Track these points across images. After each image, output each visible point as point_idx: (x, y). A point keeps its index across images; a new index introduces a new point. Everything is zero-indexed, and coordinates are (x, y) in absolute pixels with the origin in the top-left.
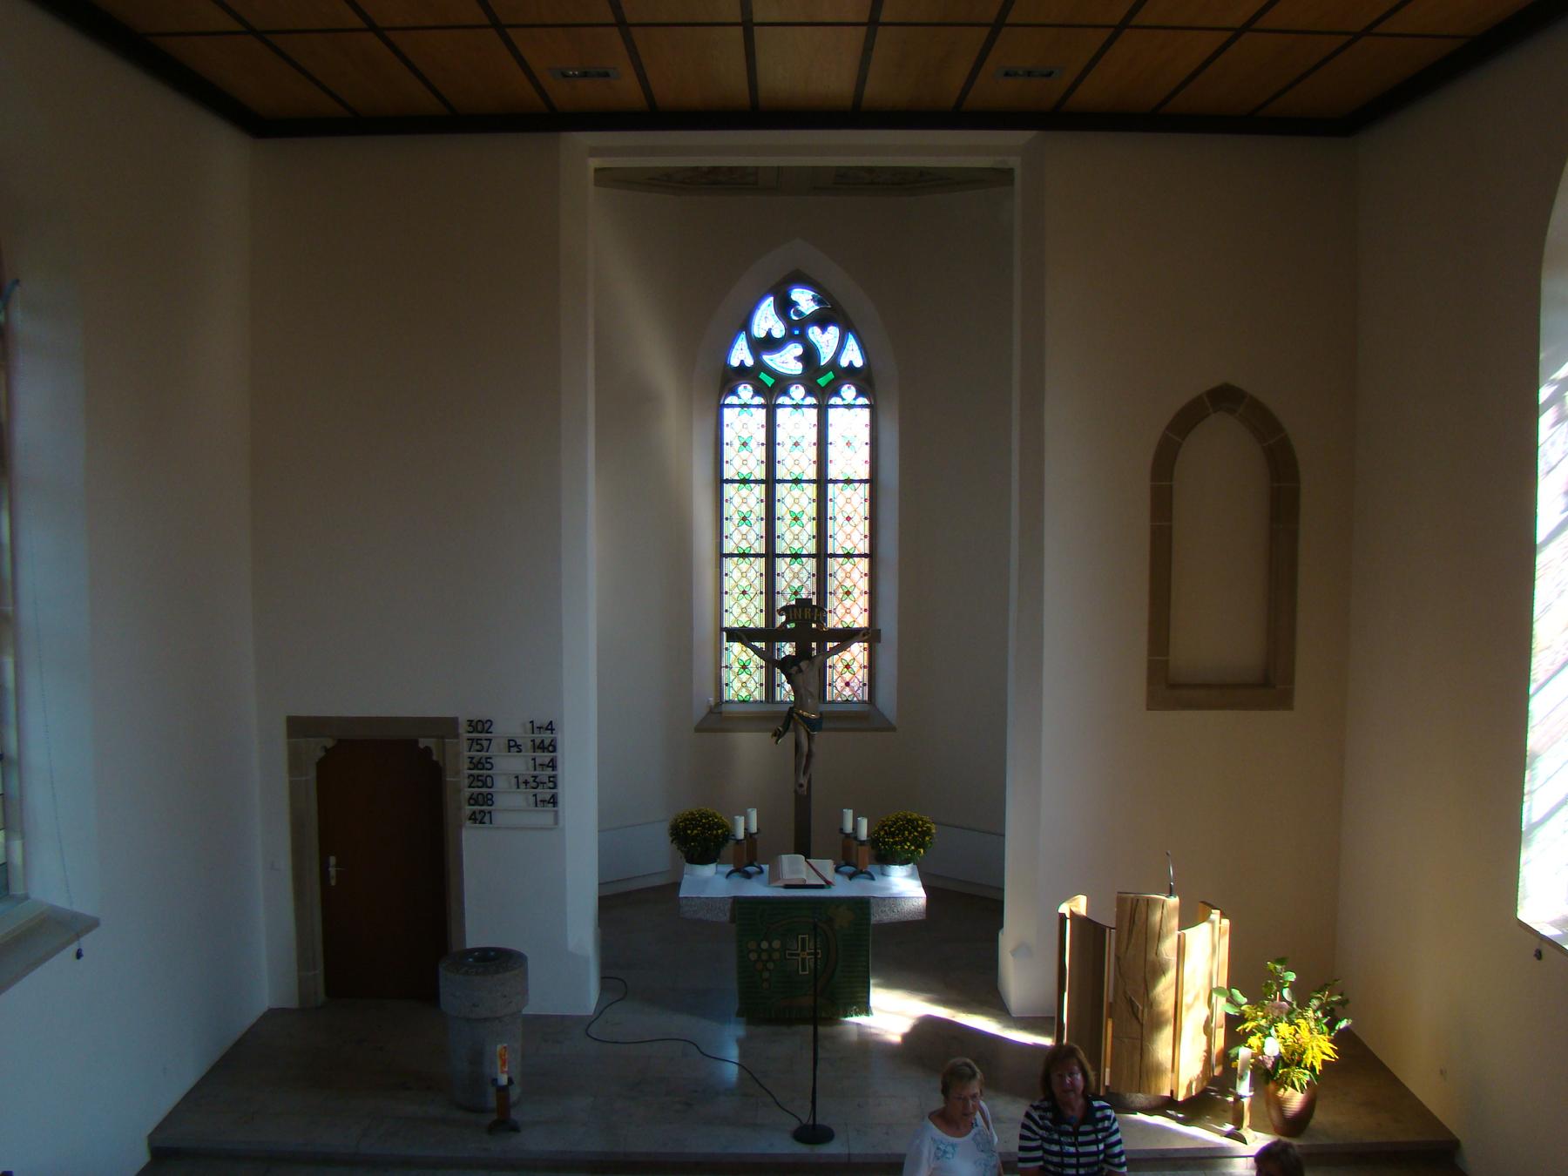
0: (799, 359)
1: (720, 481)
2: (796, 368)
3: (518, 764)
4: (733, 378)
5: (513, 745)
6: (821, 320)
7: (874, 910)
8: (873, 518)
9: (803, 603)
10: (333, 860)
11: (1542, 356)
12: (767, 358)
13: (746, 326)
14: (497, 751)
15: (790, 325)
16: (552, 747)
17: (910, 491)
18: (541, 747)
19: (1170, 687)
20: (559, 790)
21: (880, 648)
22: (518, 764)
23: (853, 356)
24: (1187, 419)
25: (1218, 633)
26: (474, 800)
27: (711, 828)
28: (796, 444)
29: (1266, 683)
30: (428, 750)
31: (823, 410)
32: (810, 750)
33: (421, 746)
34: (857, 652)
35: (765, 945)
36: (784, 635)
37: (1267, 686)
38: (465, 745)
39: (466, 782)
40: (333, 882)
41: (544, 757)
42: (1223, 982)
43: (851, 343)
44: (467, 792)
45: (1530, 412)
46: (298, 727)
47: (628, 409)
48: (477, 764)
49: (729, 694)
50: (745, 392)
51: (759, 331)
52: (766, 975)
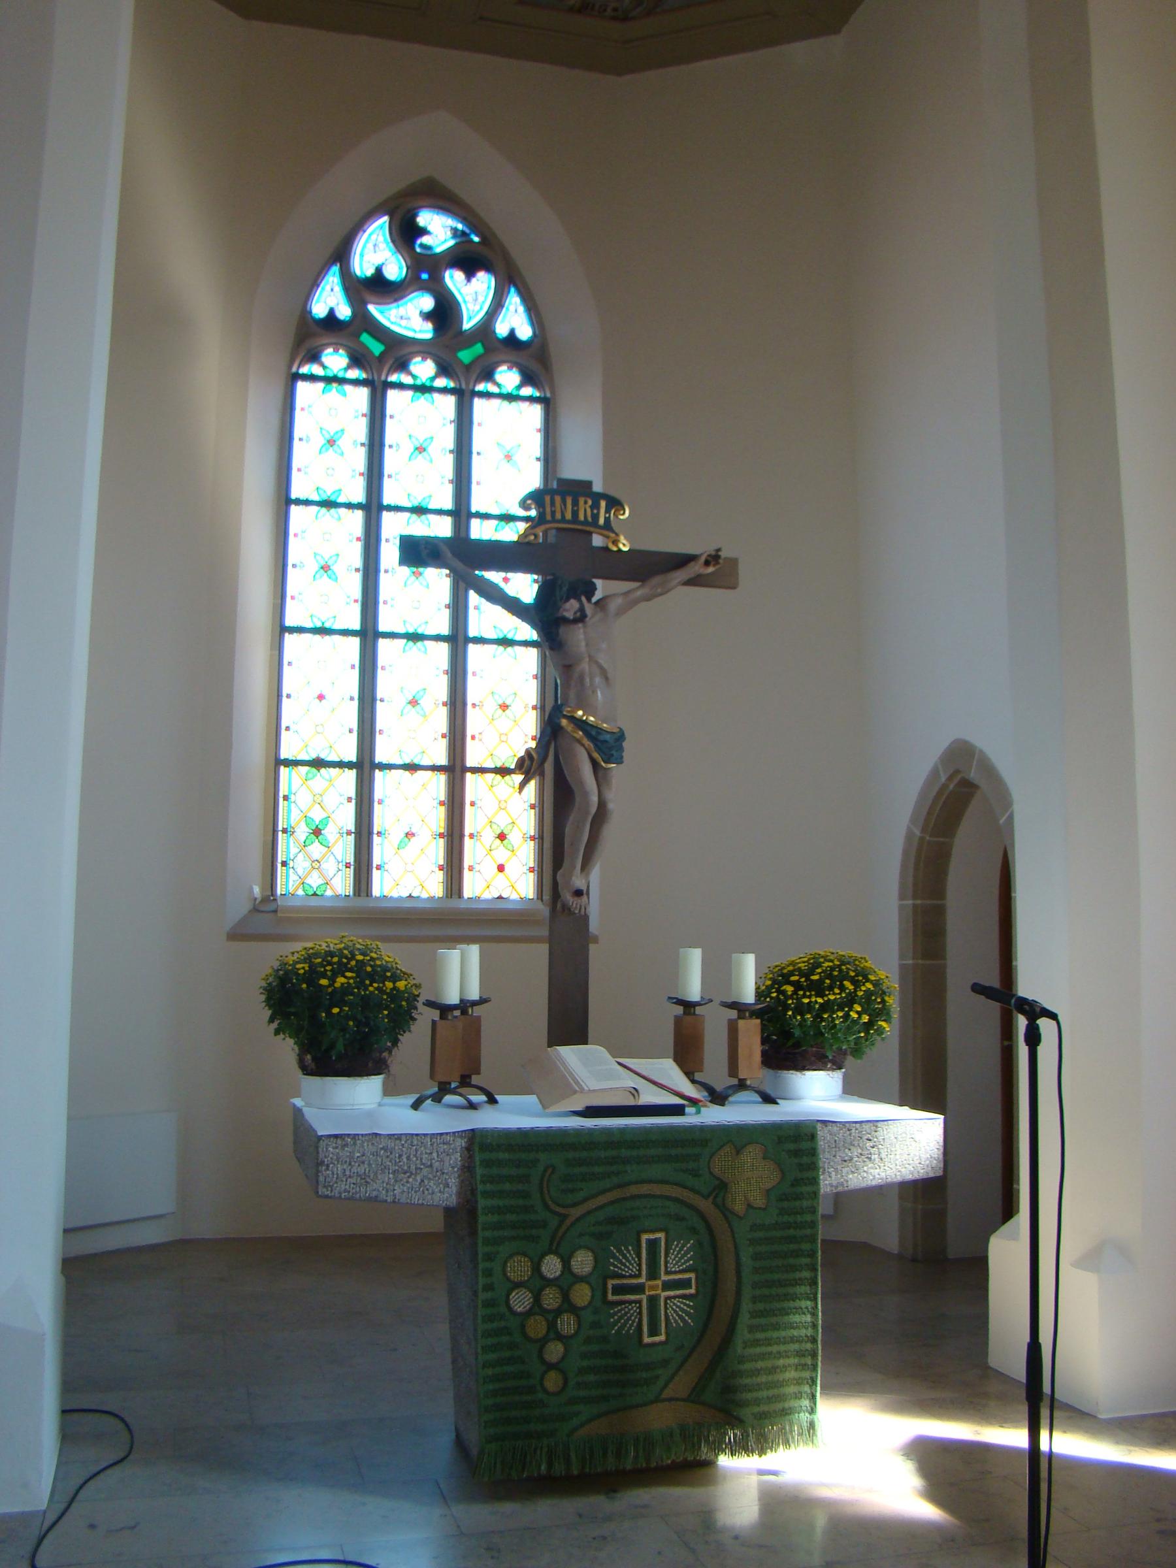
0: (428, 316)
1: (284, 501)
2: (425, 331)
4: (310, 336)
6: (468, 261)
13: (342, 255)
23: (515, 320)
32: (602, 805)
35: (552, 1266)
43: (514, 301)
49: (288, 883)
50: (335, 360)
52: (555, 1351)
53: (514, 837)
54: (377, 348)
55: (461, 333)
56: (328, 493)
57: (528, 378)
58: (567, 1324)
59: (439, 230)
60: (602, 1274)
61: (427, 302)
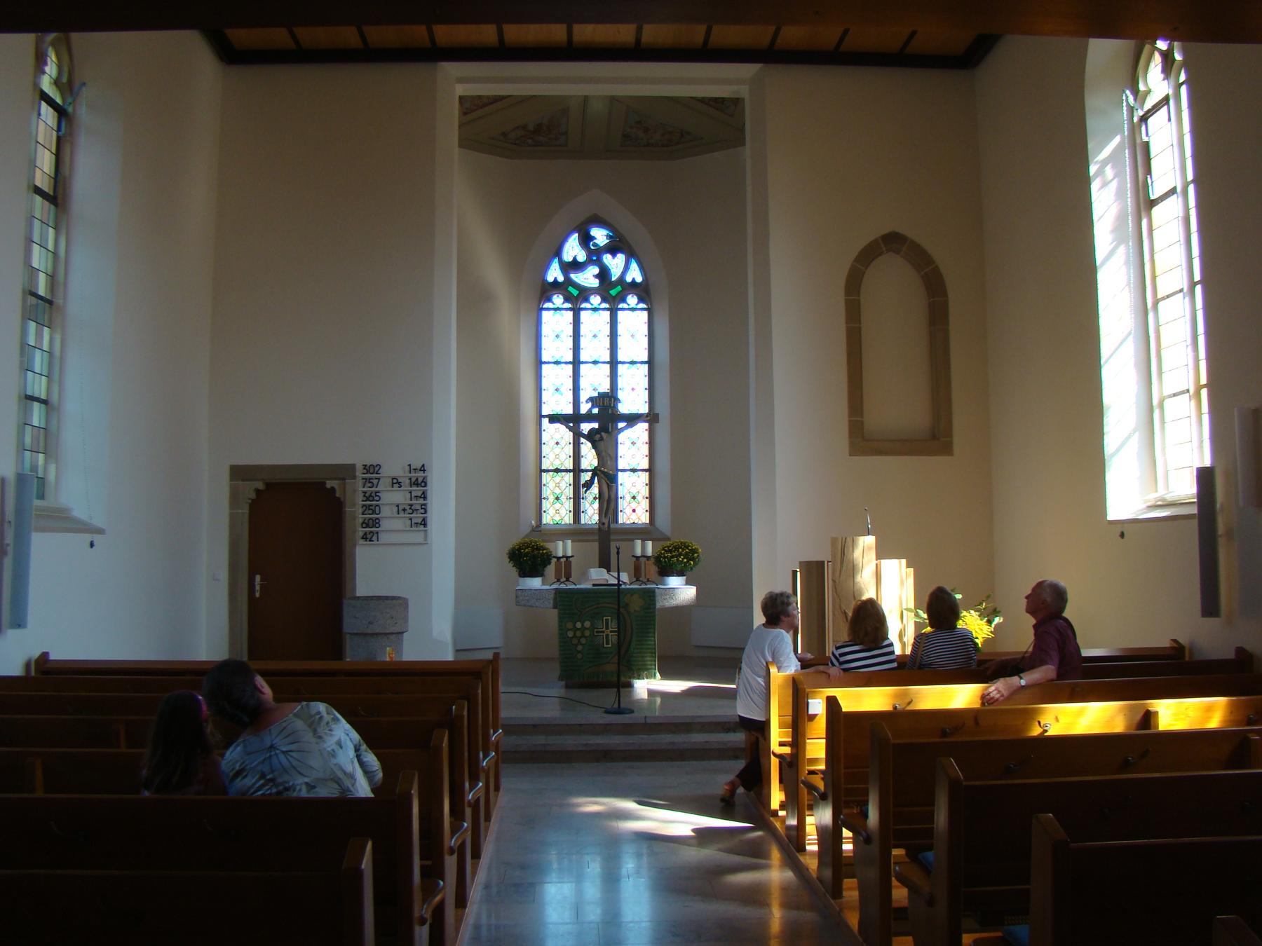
0: (596, 276)
1: (539, 363)
2: (595, 283)
3: (398, 497)
5: (395, 482)
6: (613, 249)
7: (658, 598)
8: (651, 389)
9: (602, 396)
10: (258, 578)
11: (1090, 146)
12: (573, 276)
13: (558, 253)
14: (383, 485)
15: (590, 253)
16: (424, 483)
17: (675, 365)
18: (416, 484)
19: (863, 440)
20: (428, 515)
21: (658, 426)
22: (398, 497)
23: (634, 274)
24: (868, 255)
25: (898, 402)
26: (366, 524)
27: (538, 549)
28: (595, 336)
29: (934, 437)
30: (333, 489)
31: (613, 312)
33: (328, 486)
34: (641, 429)
35: (579, 625)
36: (589, 417)
37: (935, 439)
38: (361, 482)
39: (361, 510)
40: (257, 595)
41: (417, 491)
42: (912, 605)
43: (634, 265)
44: (360, 518)
45: (1085, 181)
46: (239, 473)
47: (475, 301)
48: (368, 497)
49: (547, 519)
50: (558, 300)
51: (568, 256)
52: (580, 648)
53: (639, 498)
54: (575, 292)
55: (611, 282)
56: (558, 358)
57: (641, 300)
58: (583, 641)
59: (600, 236)
60: (593, 627)
61: (596, 270)
